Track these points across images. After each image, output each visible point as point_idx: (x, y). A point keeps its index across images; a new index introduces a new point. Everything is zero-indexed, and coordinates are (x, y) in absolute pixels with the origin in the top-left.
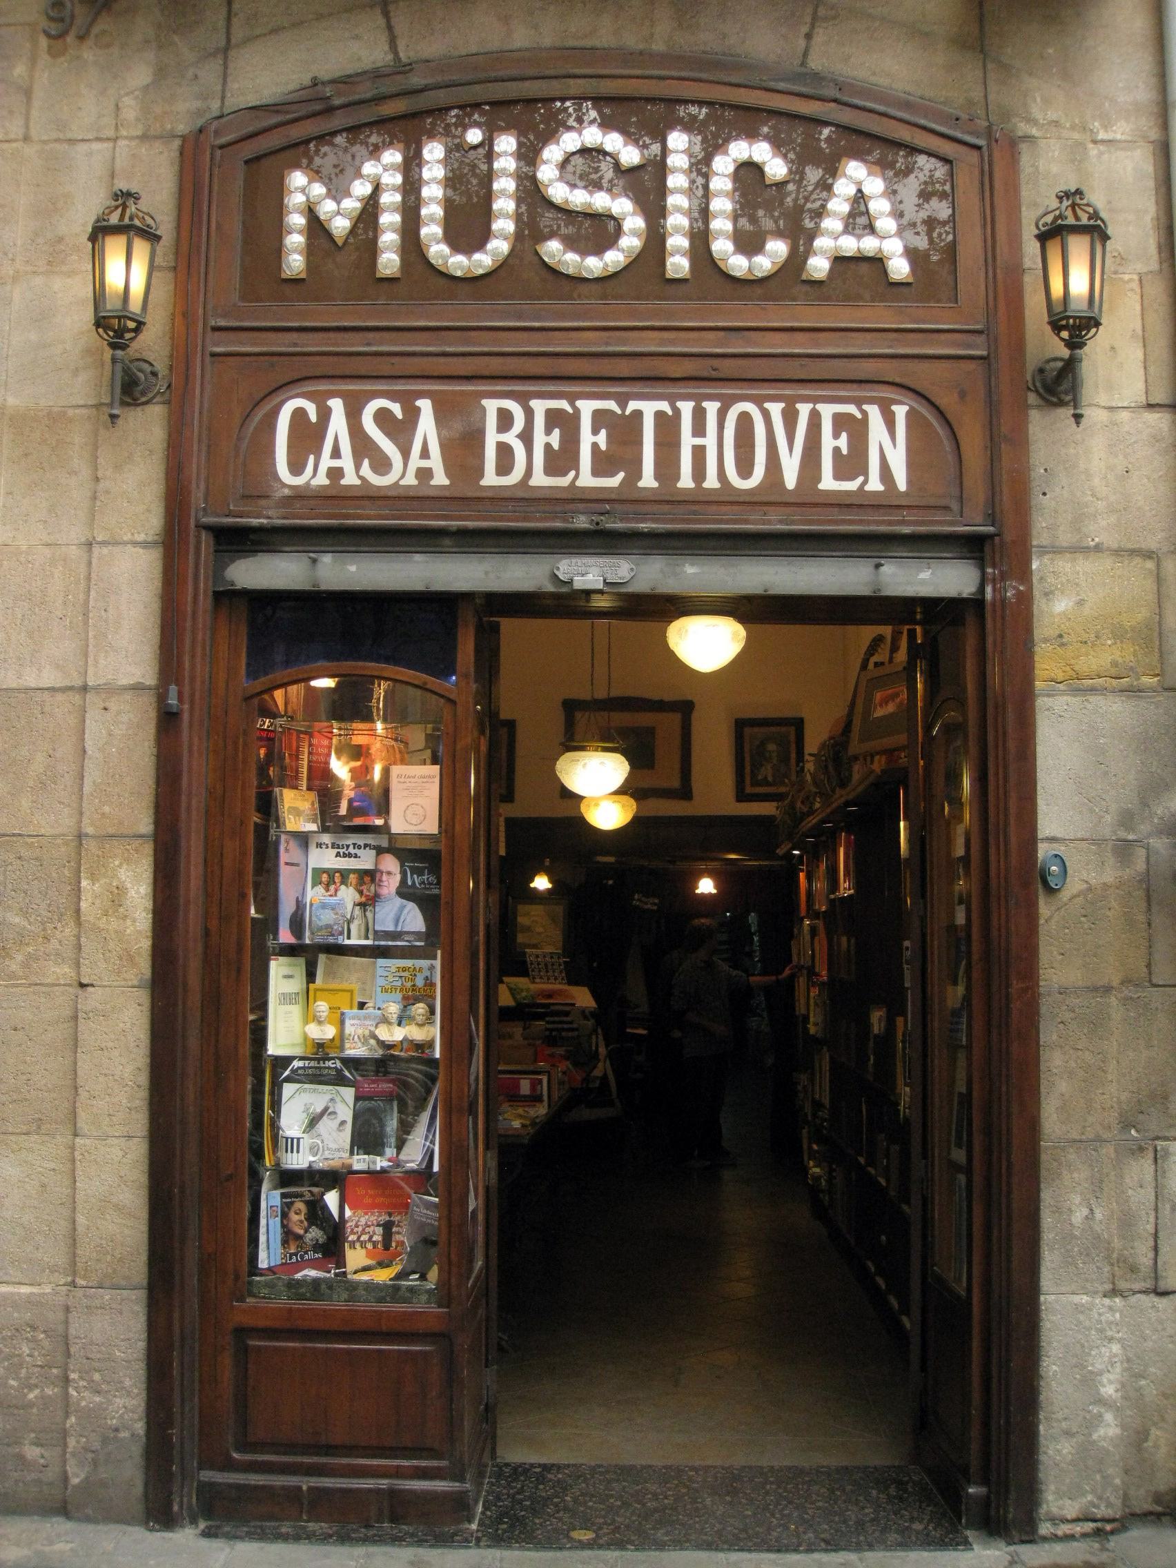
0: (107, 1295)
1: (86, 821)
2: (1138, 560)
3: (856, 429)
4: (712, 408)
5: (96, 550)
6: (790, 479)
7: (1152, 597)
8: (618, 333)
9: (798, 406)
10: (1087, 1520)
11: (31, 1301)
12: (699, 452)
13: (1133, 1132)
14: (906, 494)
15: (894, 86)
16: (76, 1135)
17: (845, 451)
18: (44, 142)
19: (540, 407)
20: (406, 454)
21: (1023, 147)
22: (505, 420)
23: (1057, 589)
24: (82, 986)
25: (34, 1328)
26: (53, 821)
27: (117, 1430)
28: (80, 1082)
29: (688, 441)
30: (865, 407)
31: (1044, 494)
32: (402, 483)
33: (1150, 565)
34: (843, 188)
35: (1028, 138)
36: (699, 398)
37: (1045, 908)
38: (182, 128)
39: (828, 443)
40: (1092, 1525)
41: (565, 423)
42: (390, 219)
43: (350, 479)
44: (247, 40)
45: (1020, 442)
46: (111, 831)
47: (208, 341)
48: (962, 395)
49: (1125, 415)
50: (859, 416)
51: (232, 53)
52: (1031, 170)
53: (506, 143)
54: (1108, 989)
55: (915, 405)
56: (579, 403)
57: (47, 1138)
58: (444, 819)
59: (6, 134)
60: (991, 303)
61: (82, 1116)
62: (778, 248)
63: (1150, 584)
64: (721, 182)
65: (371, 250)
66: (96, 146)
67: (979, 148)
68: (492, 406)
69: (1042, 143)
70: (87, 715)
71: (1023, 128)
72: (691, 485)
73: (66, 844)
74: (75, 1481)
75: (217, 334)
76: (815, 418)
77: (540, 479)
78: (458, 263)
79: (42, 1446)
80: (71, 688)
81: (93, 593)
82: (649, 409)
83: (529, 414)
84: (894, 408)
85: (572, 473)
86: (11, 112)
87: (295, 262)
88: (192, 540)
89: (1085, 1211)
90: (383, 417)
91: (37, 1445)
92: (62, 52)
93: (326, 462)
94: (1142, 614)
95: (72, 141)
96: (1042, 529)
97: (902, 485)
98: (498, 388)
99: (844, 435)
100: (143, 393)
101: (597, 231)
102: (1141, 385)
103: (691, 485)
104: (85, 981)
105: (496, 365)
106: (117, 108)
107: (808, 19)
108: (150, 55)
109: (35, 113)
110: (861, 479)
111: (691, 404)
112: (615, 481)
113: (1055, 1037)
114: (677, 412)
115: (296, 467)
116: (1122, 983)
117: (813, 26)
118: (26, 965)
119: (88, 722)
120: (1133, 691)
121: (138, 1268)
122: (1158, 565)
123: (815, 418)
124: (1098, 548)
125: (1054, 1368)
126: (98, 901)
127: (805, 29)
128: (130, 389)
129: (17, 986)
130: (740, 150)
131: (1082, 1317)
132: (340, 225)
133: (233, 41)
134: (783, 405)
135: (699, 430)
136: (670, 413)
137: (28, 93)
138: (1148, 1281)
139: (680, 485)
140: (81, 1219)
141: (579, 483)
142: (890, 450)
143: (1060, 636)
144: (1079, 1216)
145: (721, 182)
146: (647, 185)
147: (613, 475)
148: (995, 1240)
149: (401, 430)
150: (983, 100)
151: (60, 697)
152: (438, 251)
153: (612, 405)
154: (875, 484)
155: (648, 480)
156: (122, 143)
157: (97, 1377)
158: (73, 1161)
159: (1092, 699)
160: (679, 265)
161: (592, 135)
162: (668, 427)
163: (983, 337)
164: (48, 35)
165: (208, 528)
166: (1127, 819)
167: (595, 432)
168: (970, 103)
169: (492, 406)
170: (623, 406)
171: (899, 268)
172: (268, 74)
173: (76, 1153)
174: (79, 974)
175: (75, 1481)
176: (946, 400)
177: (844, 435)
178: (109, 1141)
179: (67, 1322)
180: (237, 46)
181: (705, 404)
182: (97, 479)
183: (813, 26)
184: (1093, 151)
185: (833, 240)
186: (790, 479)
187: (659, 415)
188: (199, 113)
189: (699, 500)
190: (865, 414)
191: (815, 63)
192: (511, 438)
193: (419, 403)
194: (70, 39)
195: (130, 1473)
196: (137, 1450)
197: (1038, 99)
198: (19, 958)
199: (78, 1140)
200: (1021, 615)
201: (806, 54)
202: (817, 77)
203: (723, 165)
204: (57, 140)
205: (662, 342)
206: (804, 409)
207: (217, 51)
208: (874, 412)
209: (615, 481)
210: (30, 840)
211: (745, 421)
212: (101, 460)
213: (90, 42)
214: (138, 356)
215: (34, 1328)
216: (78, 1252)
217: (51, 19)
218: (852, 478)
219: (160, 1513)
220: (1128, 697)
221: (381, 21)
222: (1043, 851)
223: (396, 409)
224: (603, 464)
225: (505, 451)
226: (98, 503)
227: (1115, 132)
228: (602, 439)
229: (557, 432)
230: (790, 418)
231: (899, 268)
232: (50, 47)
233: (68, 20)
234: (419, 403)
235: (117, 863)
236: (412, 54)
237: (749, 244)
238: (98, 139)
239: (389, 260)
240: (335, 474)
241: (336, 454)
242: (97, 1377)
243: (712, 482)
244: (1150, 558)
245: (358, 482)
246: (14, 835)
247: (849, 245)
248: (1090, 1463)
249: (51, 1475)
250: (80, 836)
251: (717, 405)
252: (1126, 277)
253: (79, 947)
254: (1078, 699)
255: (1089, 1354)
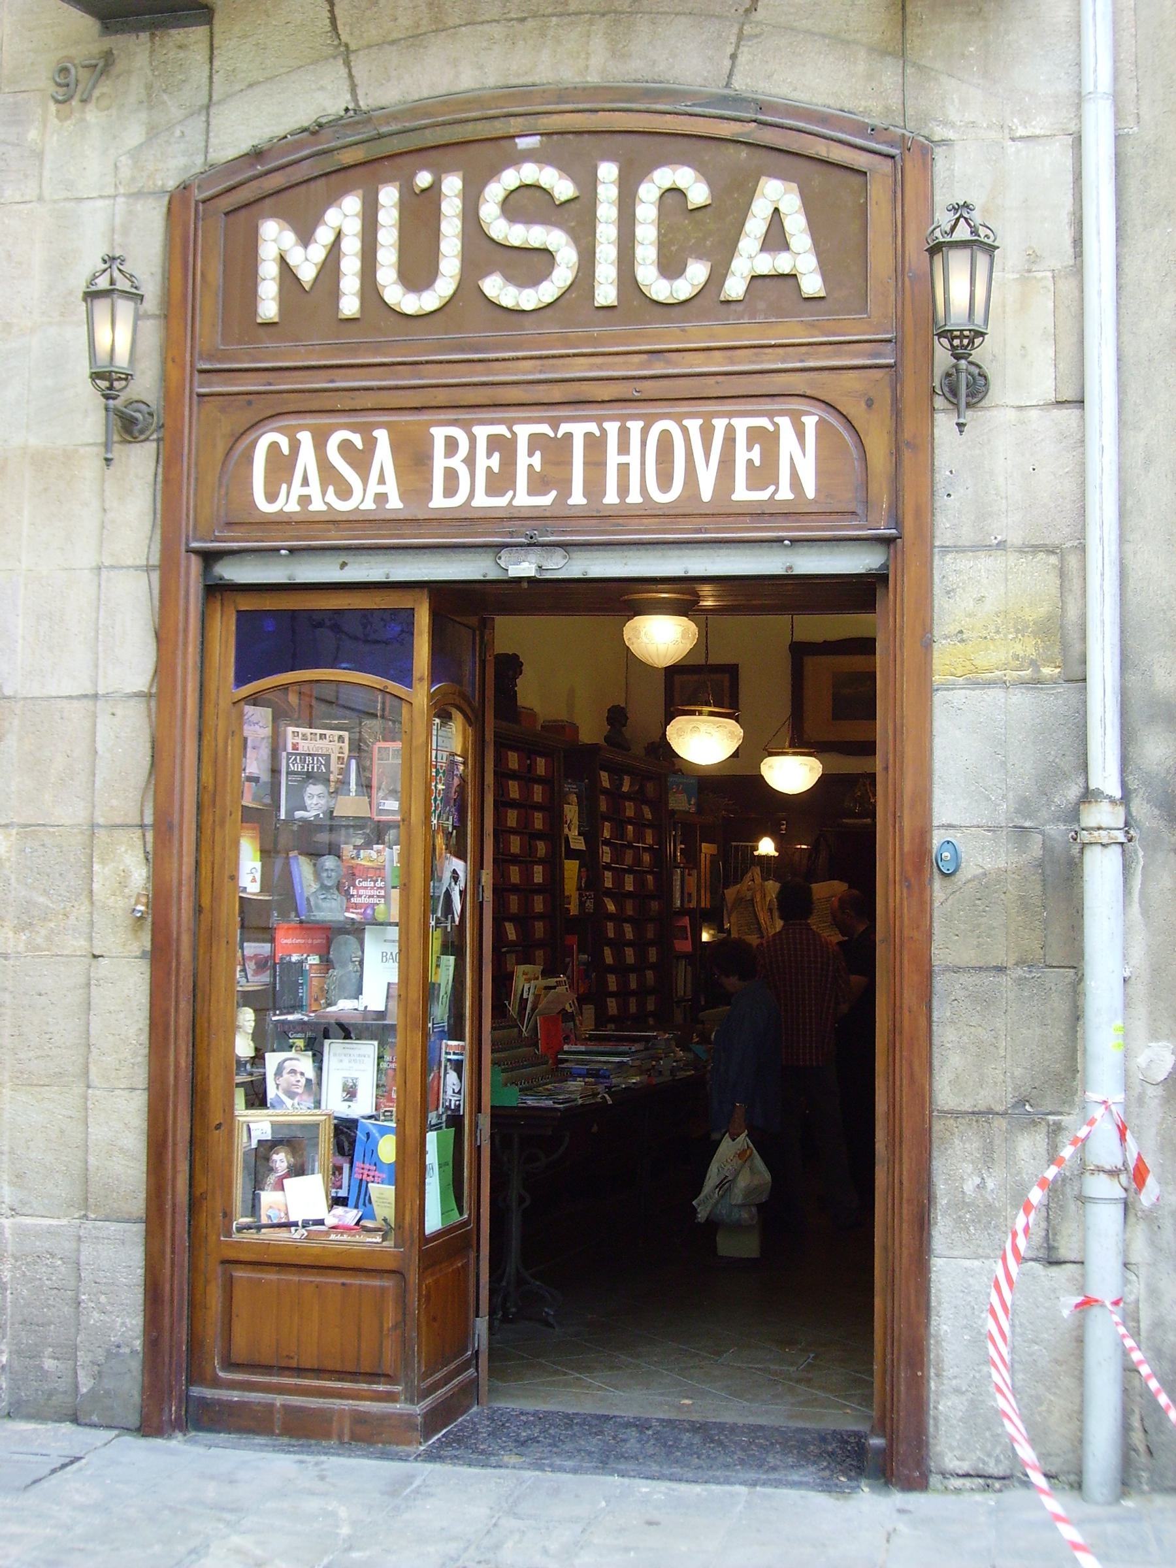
0: (113, 1226)
1: (97, 813)
2: (1042, 555)
3: (767, 440)
4: (635, 427)
5: (104, 573)
6: (706, 494)
7: (1055, 591)
8: (551, 361)
9: (715, 422)
10: (979, 1476)
11: (51, 1232)
12: (624, 469)
13: (1028, 1107)
14: (815, 501)
15: (814, 100)
16: (88, 1087)
17: (757, 463)
18: (55, 202)
19: (482, 432)
20: (365, 480)
21: (939, 153)
22: (451, 445)
23: (958, 587)
24: (95, 956)
25: (53, 1256)
26: (70, 812)
27: (118, 1346)
28: (92, 1041)
29: (613, 459)
30: (776, 419)
31: (949, 495)
32: (361, 507)
33: (1053, 560)
34: (760, 211)
35: (944, 142)
36: (623, 419)
37: (939, 890)
38: (171, 184)
39: (743, 455)
40: (981, 1481)
41: (503, 446)
42: (350, 265)
43: (317, 505)
44: (230, 96)
45: (926, 446)
46: (118, 821)
47: (196, 384)
48: (870, 403)
49: (1034, 414)
50: (771, 428)
51: (213, 111)
52: (948, 173)
53: (452, 184)
54: (1001, 969)
55: (824, 415)
56: (516, 428)
57: (65, 1089)
58: (473, 586)
59: (22, 196)
60: (899, 309)
61: (93, 1069)
62: (697, 272)
63: (1053, 581)
64: (647, 212)
65: (335, 294)
66: (100, 203)
67: (893, 157)
68: (439, 434)
69: (958, 147)
70: (98, 720)
71: (939, 132)
72: (616, 501)
73: (82, 833)
74: (84, 1390)
75: (204, 376)
76: (730, 433)
77: (482, 500)
78: (411, 303)
79: (58, 1359)
80: (86, 696)
81: (102, 613)
82: (579, 430)
83: (473, 440)
84: (804, 419)
85: (510, 493)
86: (26, 176)
87: (268, 309)
88: (183, 562)
89: (978, 1180)
90: (346, 448)
91: (55, 1358)
92: (68, 117)
93: (297, 490)
94: (1043, 610)
95: (79, 200)
96: (945, 529)
97: (810, 493)
98: (442, 417)
99: (757, 448)
100: (142, 432)
101: (532, 264)
102: (1050, 383)
103: (616, 501)
104: (97, 953)
105: (442, 397)
106: (116, 167)
107: (733, 39)
108: (143, 115)
109: (47, 174)
110: (772, 488)
111: (617, 424)
112: (547, 500)
113: (948, 1014)
114: (604, 432)
115: (271, 497)
116: (1017, 964)
117: (738, 46)
118: (48, 939)
119: (98, 726)
120: (1036, 683)
121: (138, 1205)
122: (1062, 560)
123: (730, 433)
124: (1001, 545)
125: (945, 1327)
126: (107, 883)
127: (730, 50)
128: (127, 425)
129: (40, 957)
130: (665, 176)
131: (971, 1280)
132: (307, 274)
133: (215, 98)
134: (700, 421)
135: (624, 448)
136: (598, 434)
137: (39, 156)
138: (1042, 1250)
139: (606, 501)
140: (92, 1160)
141: (515, 503)
142: (800, 459)
143: (961, 632)
144: (969, 1186)
145: (647, 212)
146: (577, 217)
147: (545, 493)
148: (229, 767)
149: (361, 460)
150: (900, 107)
151: (75, 703)
152: (394, 294)
153: (545, 429)
154: (785, 493)
155: (577, 498)
156: (120, 200)
157: (103, 1299)
158: (86, 1109)
159: (990, 692)
160: (606, 293)
161: (529, 172)
162: (595, 445)
163: (890, 346)
164: (57, 101)
165: (197, 552)
166: (1024, 807)
167: (531, 454)
168: (888, 109)
169: (439, 434)
170: (555, 429)
171: (812, 284)
172: (247, 125)
173: (89, 1103)
174: (91, 946)
175: (84, 1390)
176: (856, 411)
177: (757, 448)
178: (117, 1092)
179: (78, 1250)
180: (219, 102)
181: (629, 424)
182: (105, 510)
183: (738, 46)
184: (1011, 147)
185: (750, 259)
186: (706, 494)
187: (588, 435)
188: (186, 168)
189: (622, 515)
190: (776, 425)
191: (740, 84)
192: (456, 462)
193: (376, 433)
194: (75, 103)
195: (129, 1383)
196: (136, 1365)
197: (956, 100)
198: (43, 932)
199: (90, 1091)
200: (905, 586)
201: (730, 75)
202: (738, 100)
203: (649, 192)
204: (66, 199)
205: (592, 367)
206: (720, 424)
207: (201, 107)
208: (785, 423)
209: (547, 500)
210: (51, 830)
211: (665, 441)
212: (107, 493)
213: (91, 106)
214: (136, 397)
215: (53, 1256)
216: (91, 1189)
217: (59, 85)
218: (763, 488)
219: (150, 1426)
220: (1028, 689)
221: (343, 71)
222: (938, 838)
223: (357, 440)
224: (538, 484)
225: (451, 476)
226: (105, 532)
227: (1034, 127)
228: (537, 461)
229: (496, 455)
230: (707, 433)
231: (812, 284)
232: (58, 111)
233: (72, 86)
234: (376, 433)
235: (123, 849)
236: (370, 101)
237: (670, 267)
238: (101, 197)
239: (350, 305)
240: (305, 500)
241: (305, 482)
242: (103, 1299)
243: (635, 497)
244: (1053, 552)
245: (324, 508)
246: (39, 825)
247: (766, 264)
248: (980, 1421)
249: (62, 1385)
250: (93, 826)
251: (641, 424)
252: (1039, 275)
253: (92, 924)
254: (978, 692)
255: (979, 1317)
